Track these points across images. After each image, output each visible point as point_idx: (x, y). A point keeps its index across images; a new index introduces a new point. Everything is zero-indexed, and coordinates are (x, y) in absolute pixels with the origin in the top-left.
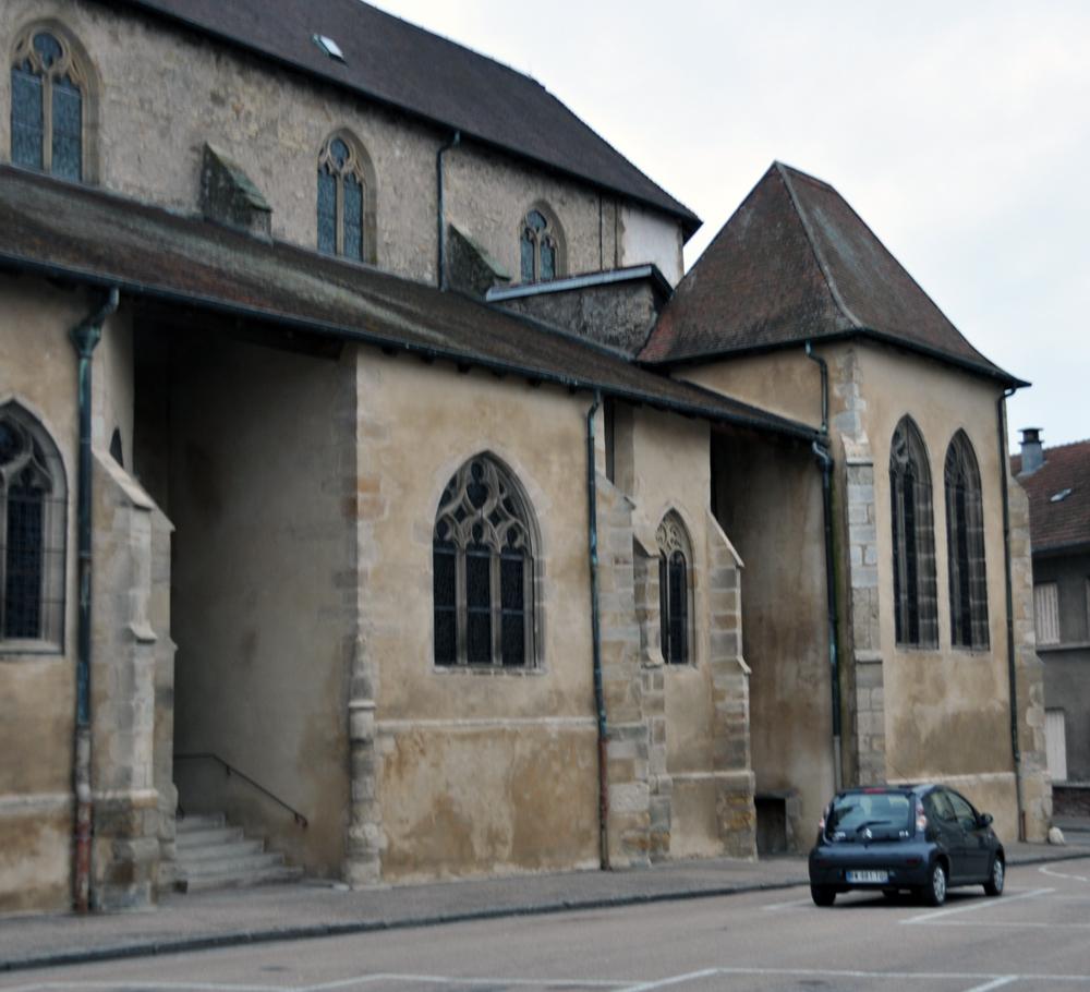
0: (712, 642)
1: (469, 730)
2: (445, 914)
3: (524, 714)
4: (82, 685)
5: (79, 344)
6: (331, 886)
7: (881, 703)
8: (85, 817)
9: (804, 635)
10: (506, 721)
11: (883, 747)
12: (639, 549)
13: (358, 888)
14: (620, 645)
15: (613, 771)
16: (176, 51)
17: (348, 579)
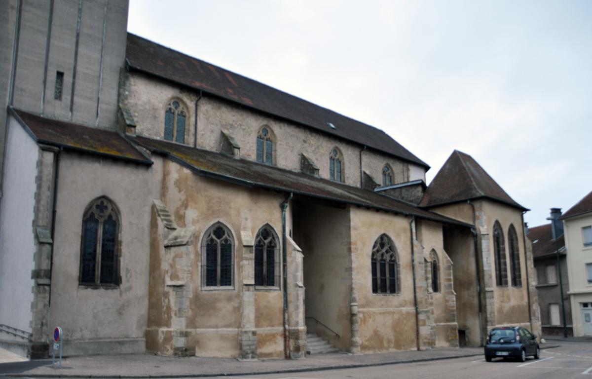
0: (445, 286)
1: (382, 311)
2: (383, 362)
3: (396, 307)
4: (285, 299)
5: (282, 208)
6: (347, 354)
7: (493, 303)
8: (287, 334)
9: (470, 284)
10: (391, 309)
11: (494, 315)
12: (426, 261)
13: (355, 355)
14: (421, 287)
15: (421, 323)
16: (295, 130)
17: (349, 270)
